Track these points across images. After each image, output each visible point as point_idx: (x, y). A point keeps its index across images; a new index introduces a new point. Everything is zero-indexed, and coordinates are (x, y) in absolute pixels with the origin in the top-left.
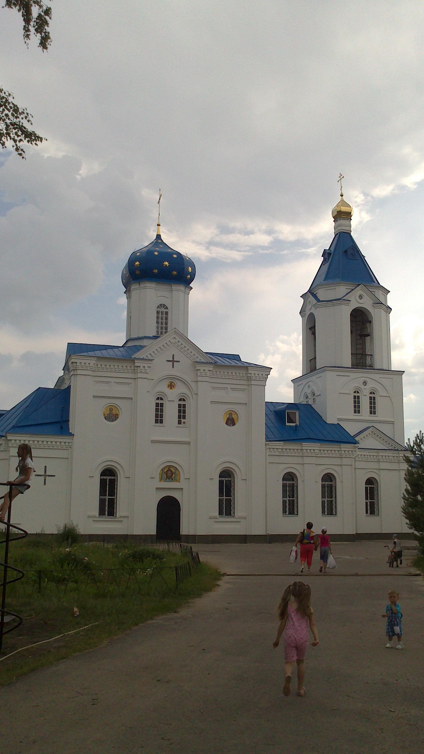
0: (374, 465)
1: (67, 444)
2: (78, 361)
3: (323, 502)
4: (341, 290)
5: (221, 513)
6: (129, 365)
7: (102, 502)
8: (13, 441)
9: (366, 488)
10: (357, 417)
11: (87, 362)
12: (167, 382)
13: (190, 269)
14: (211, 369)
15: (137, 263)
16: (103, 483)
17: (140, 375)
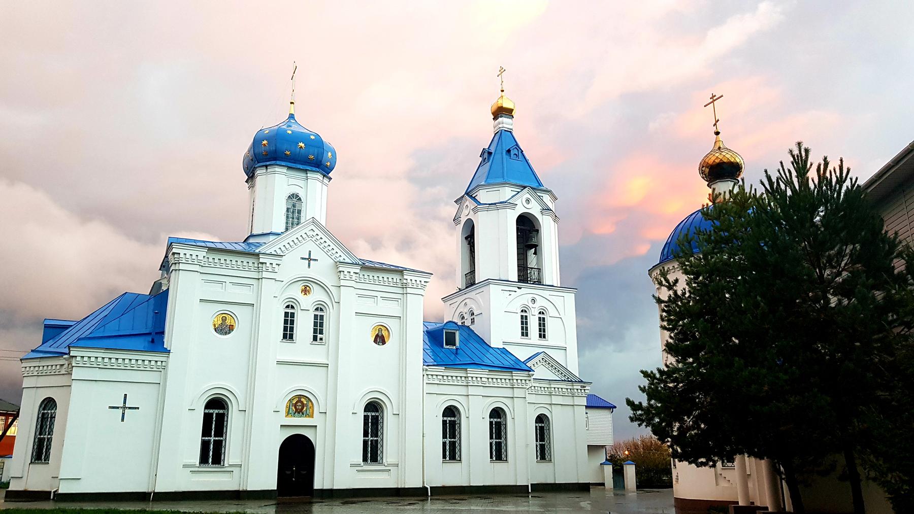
0: (546, 400)
1: (159, 363)
2: (182, 252)
3: (444, 444)
4: (506, 193)
5: (365, 459)
6: (251, 261)
7: (205, 446)
8: (79, 359)
9: (444, 422)
10: (525, 340)
11: (194, 253)
12: (300, 286)
13: (330, 154)
14: (358, 271)
15: (265, 142)
16: (207, 418)
17: (265, 275)
